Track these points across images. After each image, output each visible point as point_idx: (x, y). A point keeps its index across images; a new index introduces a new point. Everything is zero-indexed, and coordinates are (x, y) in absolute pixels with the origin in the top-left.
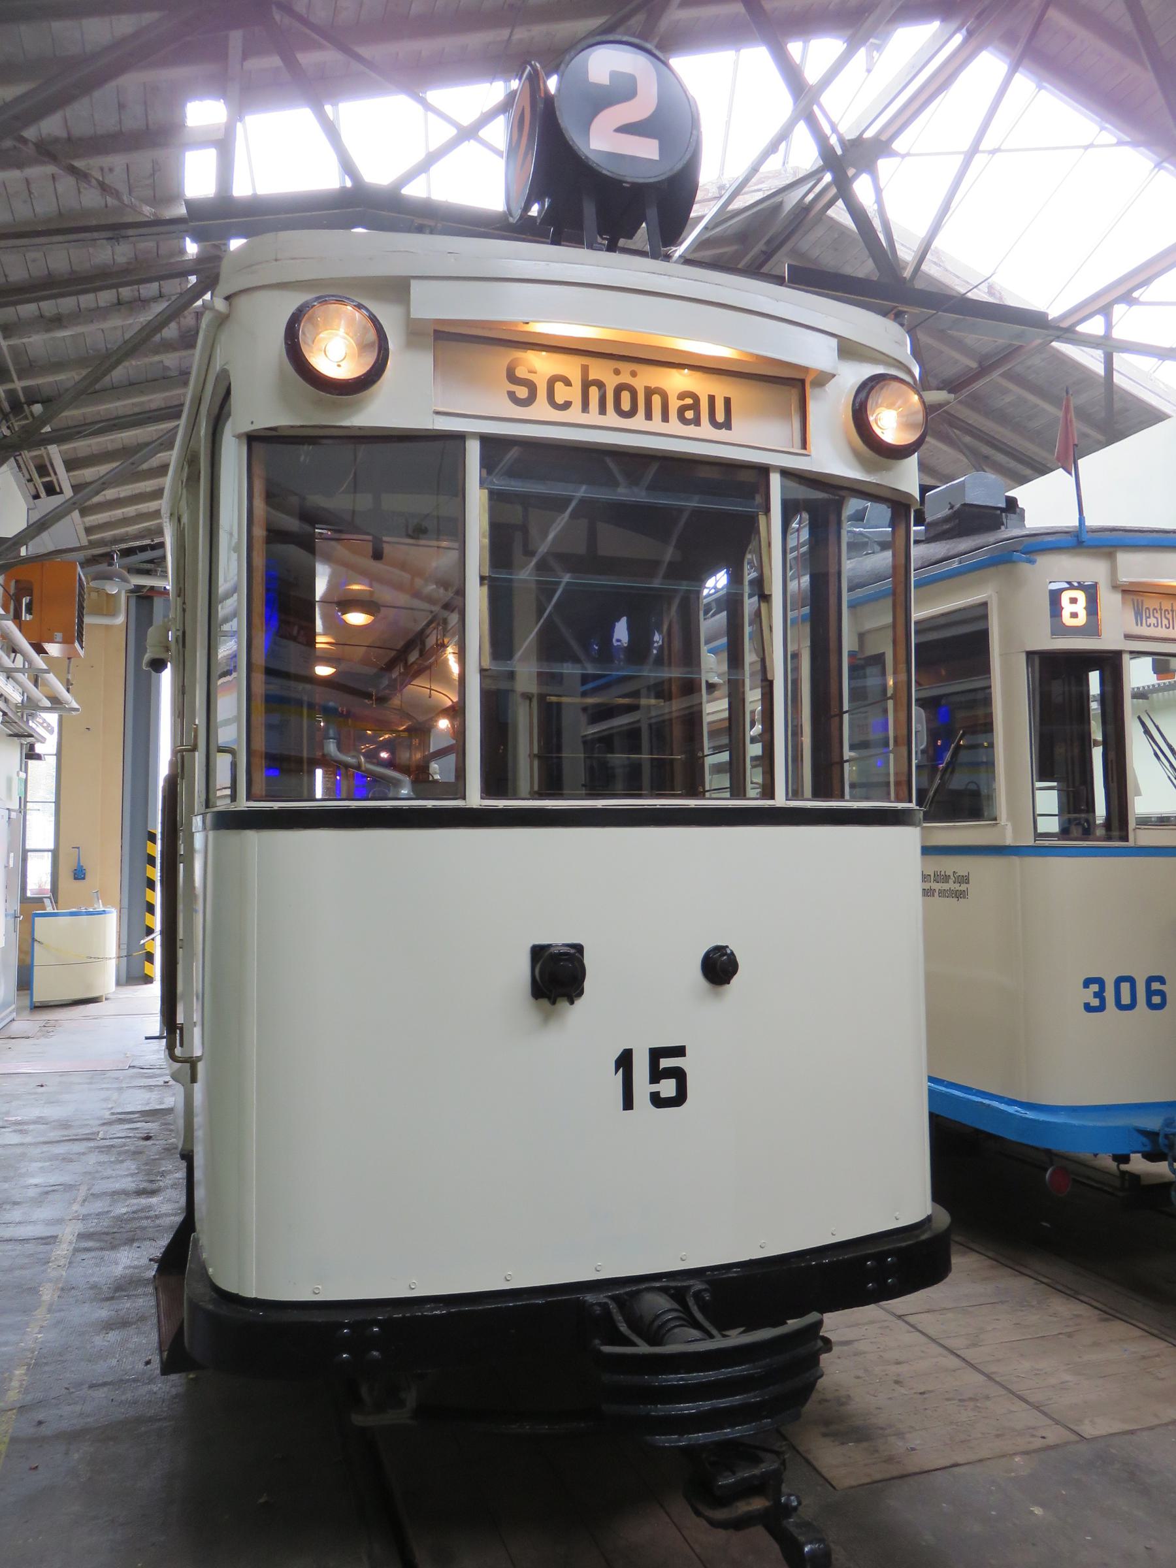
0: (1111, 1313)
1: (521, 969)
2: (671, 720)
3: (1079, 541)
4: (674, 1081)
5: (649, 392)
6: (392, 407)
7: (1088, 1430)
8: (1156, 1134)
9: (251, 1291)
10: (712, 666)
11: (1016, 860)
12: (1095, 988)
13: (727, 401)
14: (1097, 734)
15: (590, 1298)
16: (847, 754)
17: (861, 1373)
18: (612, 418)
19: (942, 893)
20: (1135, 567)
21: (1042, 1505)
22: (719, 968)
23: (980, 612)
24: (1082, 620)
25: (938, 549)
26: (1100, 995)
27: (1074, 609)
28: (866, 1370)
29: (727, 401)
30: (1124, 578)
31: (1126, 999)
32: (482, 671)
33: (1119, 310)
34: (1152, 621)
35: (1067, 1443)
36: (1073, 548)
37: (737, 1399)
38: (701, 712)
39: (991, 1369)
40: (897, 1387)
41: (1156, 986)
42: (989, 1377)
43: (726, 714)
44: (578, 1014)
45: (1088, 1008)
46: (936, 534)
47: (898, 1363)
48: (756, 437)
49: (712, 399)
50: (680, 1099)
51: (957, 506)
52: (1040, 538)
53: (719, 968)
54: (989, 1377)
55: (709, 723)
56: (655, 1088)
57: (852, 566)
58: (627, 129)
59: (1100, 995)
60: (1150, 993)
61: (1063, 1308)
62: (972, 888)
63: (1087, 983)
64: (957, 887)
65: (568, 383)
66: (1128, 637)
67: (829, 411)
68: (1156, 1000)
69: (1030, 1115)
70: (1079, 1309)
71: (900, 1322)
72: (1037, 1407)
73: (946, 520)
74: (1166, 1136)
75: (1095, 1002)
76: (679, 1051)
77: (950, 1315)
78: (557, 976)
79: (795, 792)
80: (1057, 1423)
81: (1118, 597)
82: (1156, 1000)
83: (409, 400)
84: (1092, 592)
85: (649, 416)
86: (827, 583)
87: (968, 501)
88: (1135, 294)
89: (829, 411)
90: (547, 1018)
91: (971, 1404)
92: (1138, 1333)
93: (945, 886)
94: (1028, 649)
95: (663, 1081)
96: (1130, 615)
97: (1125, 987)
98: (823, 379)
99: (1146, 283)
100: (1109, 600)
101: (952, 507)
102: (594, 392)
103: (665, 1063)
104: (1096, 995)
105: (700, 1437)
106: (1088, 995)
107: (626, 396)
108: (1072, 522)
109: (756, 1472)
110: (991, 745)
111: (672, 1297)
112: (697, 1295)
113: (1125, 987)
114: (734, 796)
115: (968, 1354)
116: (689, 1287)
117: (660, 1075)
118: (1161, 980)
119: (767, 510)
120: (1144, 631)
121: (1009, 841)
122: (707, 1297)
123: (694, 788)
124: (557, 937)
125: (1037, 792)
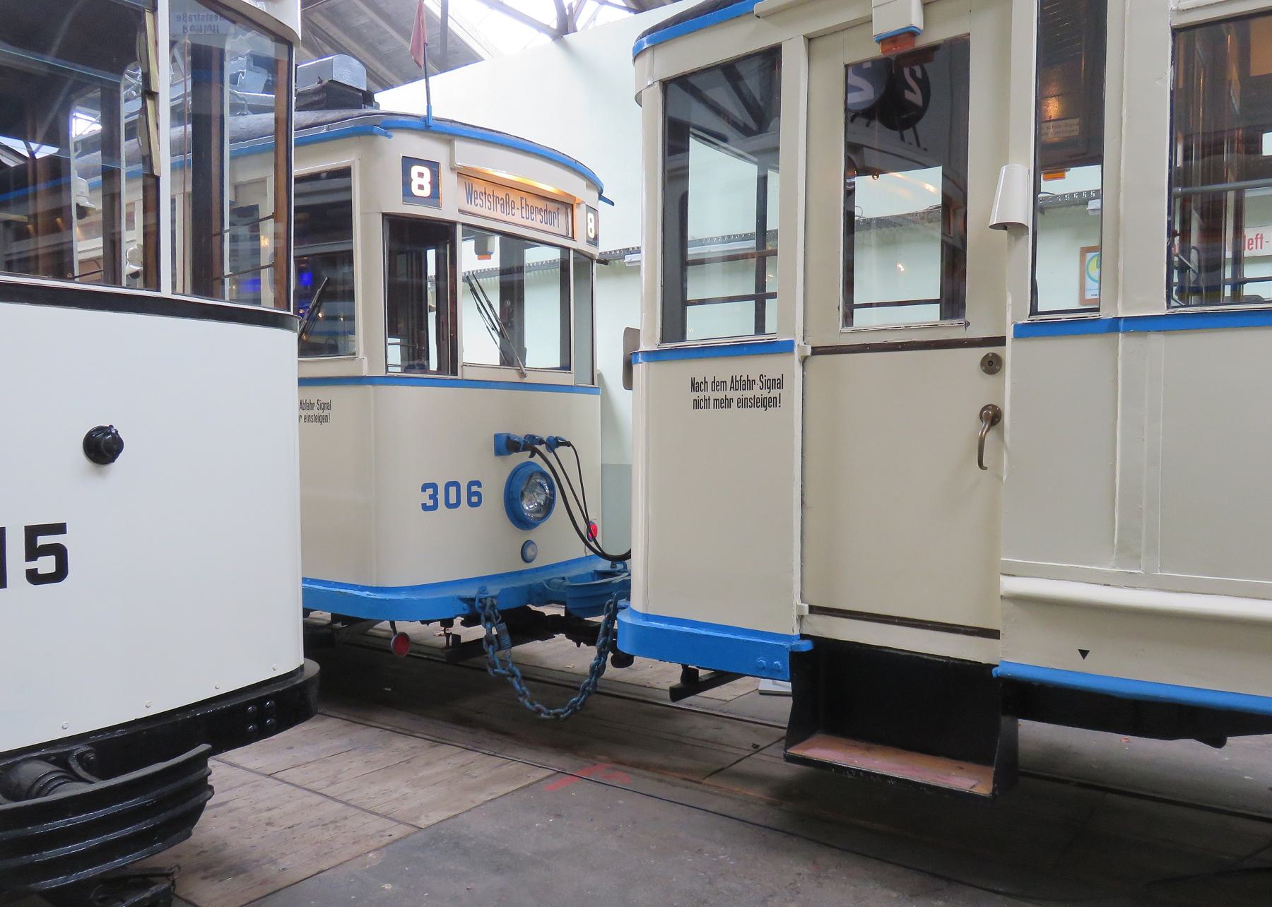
0: (438, 741)
2: (37, 257)
3: (425, 126)
4: (53, 557)
7: (423, 822)
8: (473, 600)
11: (370, 389)
12: (430, 491)
14: (432, 302)
17: (236, 824)
20: (468, 155)
21: (390, 881)
22: (102, 447)
23: (345, 173)
24: (426, 192)
26: (433, 496)
27: (421, 180)
28: (240, 821)
34: (479, 201)
35: (406, 837)
36: (422, 130)
37: (129, 830)
38: (72, 250)
39: (345, 799)
40: (269, 828)
41: (474, 488)
42: (346, 803)
45: (425, 508)
46: (307, 104)
47: (269, 809)
50: (60, 573)
51: (326, 81)
53: (102, 447)
54: (346, 803)
55: (81, 262)
56: (32, 565)
57: (234, 124)
59: (433, 496)
60: (470, 494)
61: (402, 744)
62: (333, 413)
63: (425, 487)
64: (320, 413)
68: (475, 499)
69: (379, 596)
70: (413, 742)
71: (270, 780)
72: (385, 816)
73: (316, 92)
74: (480, 601)
75: (430, 503)
76: (60, 529)
77: (313, 766)
80: (400, 823)
81: (454, 177)
82: (475, 499)
84: (434, 166)
86: (209, 125)
91: (332, 826)
92: (457, 750)
94: (385, 211)
95: (40, 558)
96: (462, 194)
97: (453, 490)
100: (448, 180)
101: (320, 82)
103: (42, 540)
104: (431, 497)
105: (90, 872)
106: (425, 498)
108: (422, 112)
109: (147, 895)
110: (351, 318)
111: (53, 763)
112: (80, 758)
113: (453, 490)
115: (327, 791)
116: (71, 752)
118: (478, 484)
121: (365, 373)
122: (92, 757)
125: (389, 347)
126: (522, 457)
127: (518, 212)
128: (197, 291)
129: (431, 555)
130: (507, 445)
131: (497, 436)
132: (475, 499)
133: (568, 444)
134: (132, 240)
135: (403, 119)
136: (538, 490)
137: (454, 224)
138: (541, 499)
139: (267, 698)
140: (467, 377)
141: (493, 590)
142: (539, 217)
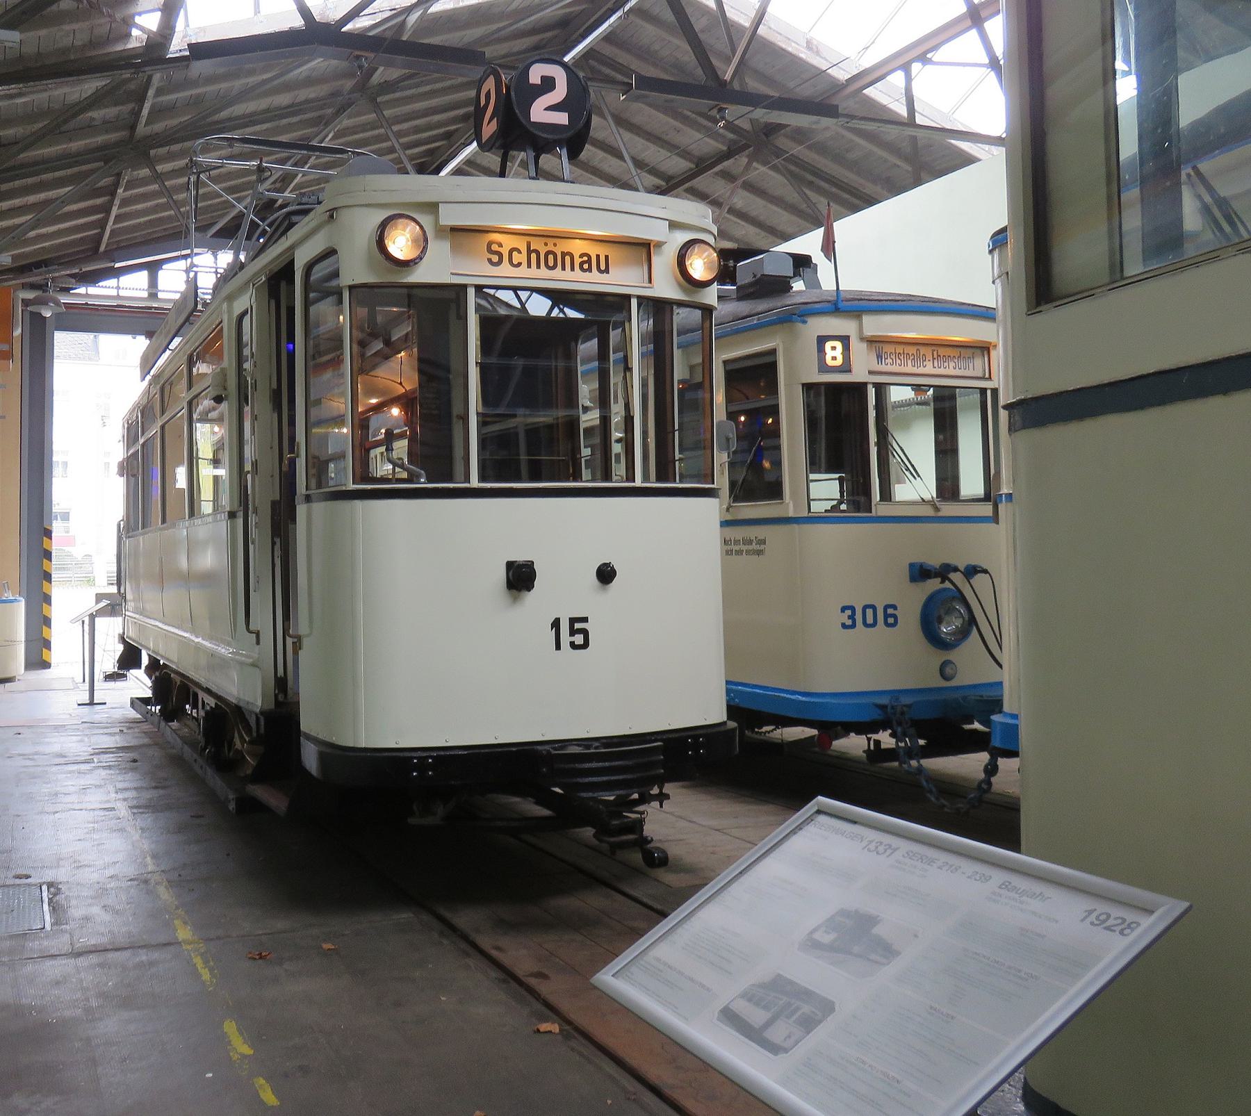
1: (501, 574)
5: (564, 255)
6: (429, 273)
9: (363, 744)
10: (586, 390)
12: (849, 612)
13: (607, 257)
15: (539, 748)
16: (677, 456)
18: (544, 272)
19: (748, 552)
20: (875, 325)
22: (606, 574)
23: (773, 352)
25: (744, 307)
26: (852, 617)
29: (607, 257)
30: (868, 332)
31: (870, 620)
32: (478, 414)
33: (916, 67)
34: (889, 361)
41: (890, 611)
43: (597, 422)
44: (530, 598)
45: (844, 626)
48: (622, 279)
49: (598, 256)
50: (585, 645)
52: (809, 306)
53: (606, 574)
56: (572, 639)
58: (549, 109)
59: (852, 617)
60: (886, 616)
62: (767, 547)
63: (843, 609)
64: (758, 547)
65: (520, 252)
66: (870, 372)
67: (664, 262)
68: (891, 620)
73: (751, 285)
75: (849, 622)
76: (585, 620)
78: (520, 578)
79: (646, 478)
82: (891, 620)
83: (439, 268)
84: (845, 340)
85: (564, 268)
87: (766, 273)
88: (929, 56)
89: (664, 262)
90: (515, 599)
93: (750, 547)
97: (869, 612)
98: (659, 245)
99: (935, 48)
100: (857, 346)
102: (534, 256)
103: (577, 626)
104: (849, 617)
106: (844, 618)
107: (551, 257)
113: (869, 612)
114: (628, 480)
117: (576, 632)
118: (894, 607)
119: (630, 320)
120: (882, 368)
121: (791, 514)
123: (577, 476)
124: (520, 557)
126: (934, 584)
127: (929, 364)
128: (659, 478)
129: (851, 664)
130: (920, 573)
131: (912, 565)
132: (891, 617)
133: (986, 572)
134: (617, 418)
135: (817, 306)
136: (957, 614)
137: (865, 384)
138: (958, 623)
139: (701, 736)
140: (880, 514)
141: (906, 700)
142: (952, 364)
